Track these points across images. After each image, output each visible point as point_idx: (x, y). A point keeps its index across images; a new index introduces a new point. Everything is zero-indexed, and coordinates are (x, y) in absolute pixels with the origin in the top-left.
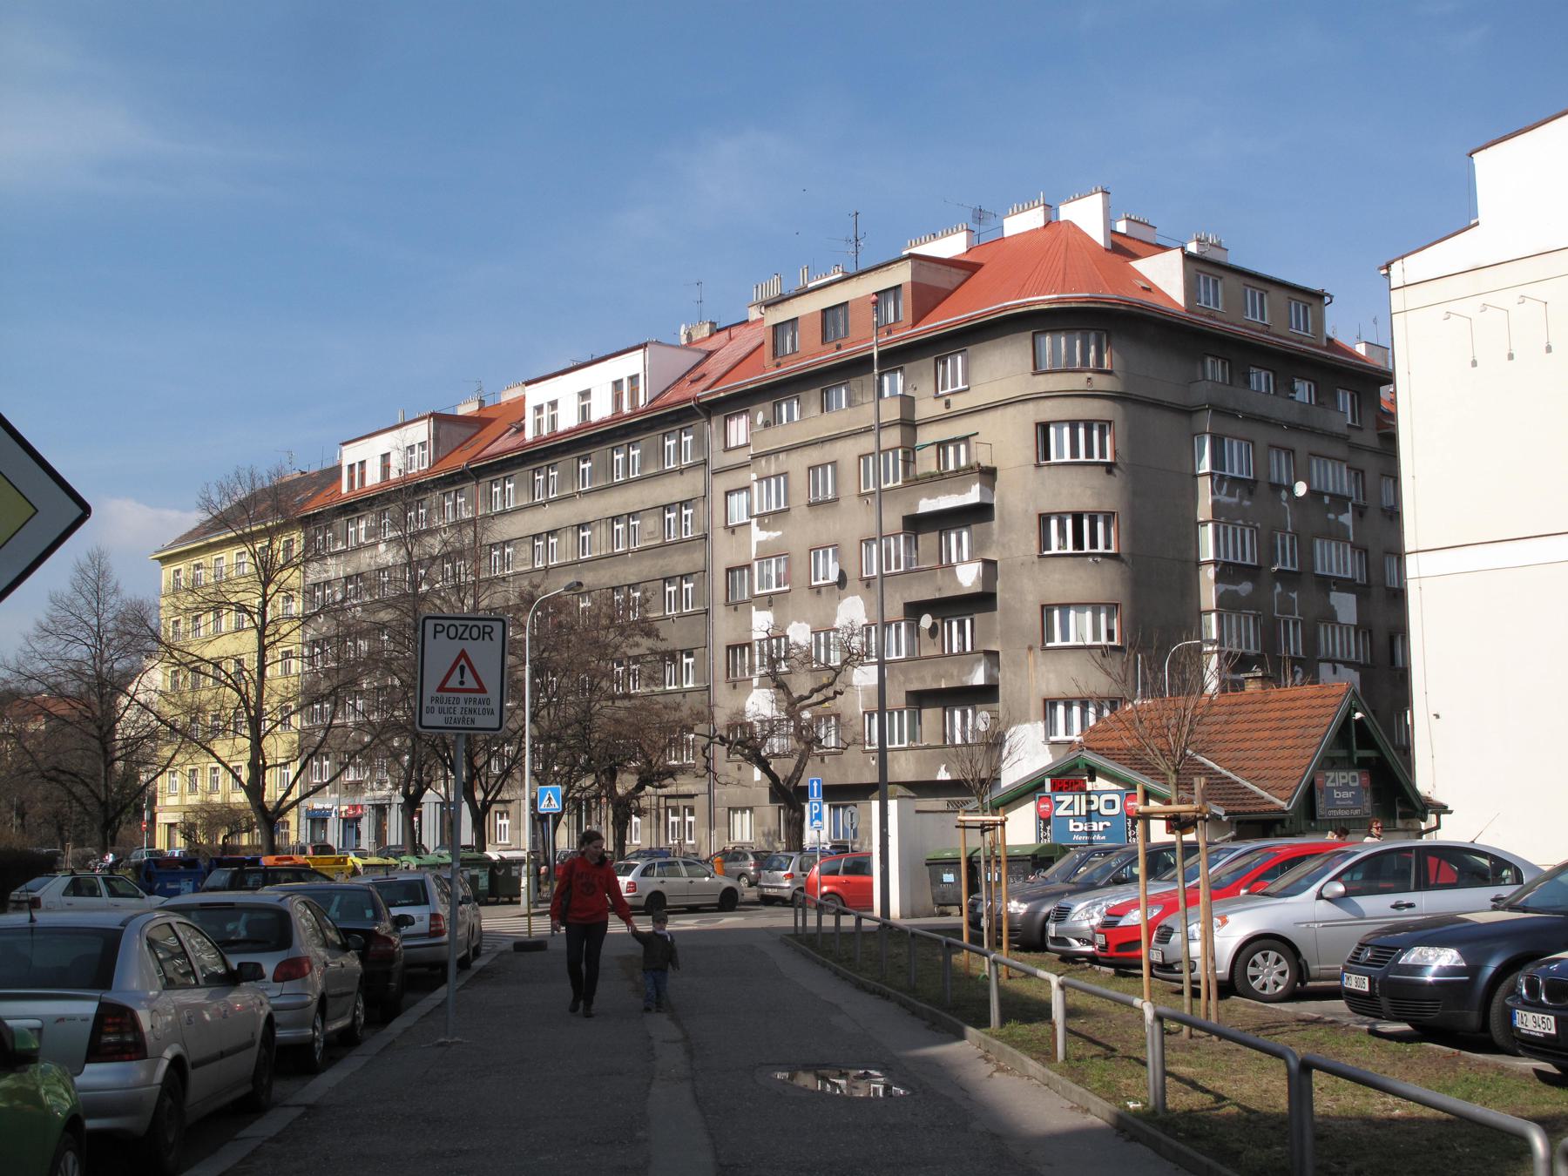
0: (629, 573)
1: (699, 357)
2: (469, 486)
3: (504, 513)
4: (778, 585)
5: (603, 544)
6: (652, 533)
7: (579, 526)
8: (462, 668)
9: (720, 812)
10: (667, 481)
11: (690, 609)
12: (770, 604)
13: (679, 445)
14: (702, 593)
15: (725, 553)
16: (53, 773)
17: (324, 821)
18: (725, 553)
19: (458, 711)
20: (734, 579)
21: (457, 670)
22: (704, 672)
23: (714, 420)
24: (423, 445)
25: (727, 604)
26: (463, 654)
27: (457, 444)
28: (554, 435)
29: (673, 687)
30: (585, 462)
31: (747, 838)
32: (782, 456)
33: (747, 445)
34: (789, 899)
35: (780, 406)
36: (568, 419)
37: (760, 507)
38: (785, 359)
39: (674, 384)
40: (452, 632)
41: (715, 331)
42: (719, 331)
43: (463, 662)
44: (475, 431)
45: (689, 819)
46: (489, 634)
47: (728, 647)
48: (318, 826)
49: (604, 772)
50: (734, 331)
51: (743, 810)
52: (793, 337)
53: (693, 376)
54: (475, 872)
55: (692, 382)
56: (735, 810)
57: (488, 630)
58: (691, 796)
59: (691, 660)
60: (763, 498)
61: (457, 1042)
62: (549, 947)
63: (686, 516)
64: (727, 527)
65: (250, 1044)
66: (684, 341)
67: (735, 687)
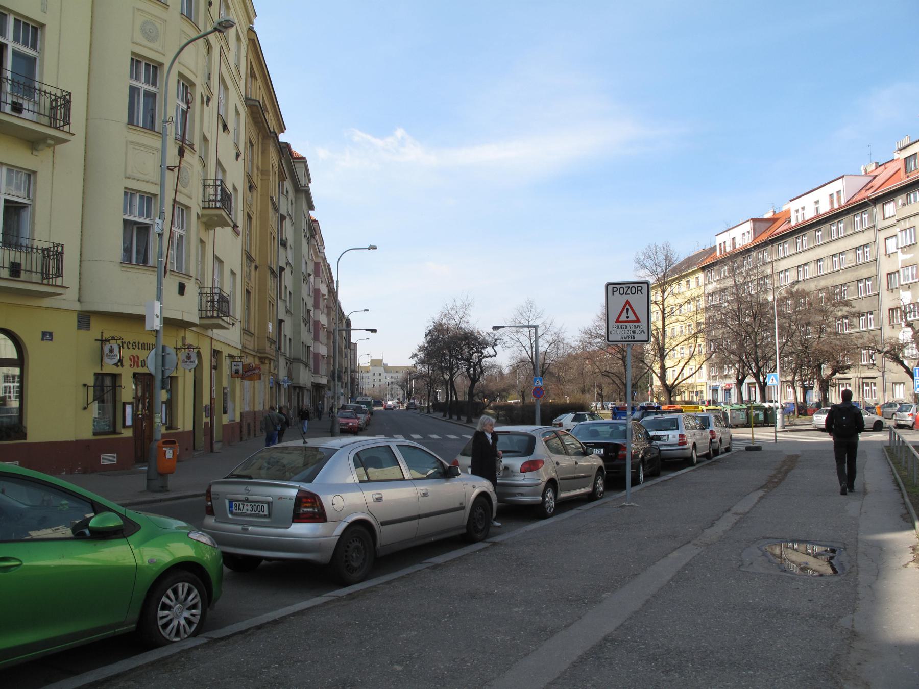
0: (840, 279)
1: (870, 178)
2: (769, 247)
3: (784, 258)
4: (913, 279)
5: (829, 267)
6: (851, 260)
7: (817, 260)
8: (628, 310)
9: (889, 385)
10: (857, 236)
11: (871, 293)
12: (909, 288)
13: (862, 220)
14: (876, 286)
15: (886, 266)
16: (606, 373)
17: (717, 390)
18: (886, 266)
19: (626, 332)
20: (891, 278)
21: (625, 311)
22: (879, 322)
23: (878, 206)
24: (748, 232)
25: (888, 289)
26: (628, 302)
27: (763, 230)
28: (804, 222)
29: (864, 329)
30: (819, 232)
31: (902, 397)
32: (912, 219)
33: (894, 216)
34: (911, 426)
35: (910, 195)
36: (810, 214)
37: (902, 243)
38: (911, 173)
39: (858, 192)
40: (622, 292)
41: (878, 166)
42: (880, 166)
43: (628, 306)
44: (771, 224)
45: (874, 388)
46: (640, 290)
47: (890, 310)
48: (714, 392)
49: (815, 367)
50: (887, 166)
51: (900, 384)
52: (915, 162)
53: (867, 188)
54: (757, 412)
55: (867, 190)
56: (896, 384)
57: (640, 288)
58: (874, 378)
59: (872, 317)
60: (904, 240)
61: (632, 506)
62: (763, 449)
63: (867, 252)
64: (886, 254)
65: (462, 508)
66: (863, 173)
67: (893, 327)
